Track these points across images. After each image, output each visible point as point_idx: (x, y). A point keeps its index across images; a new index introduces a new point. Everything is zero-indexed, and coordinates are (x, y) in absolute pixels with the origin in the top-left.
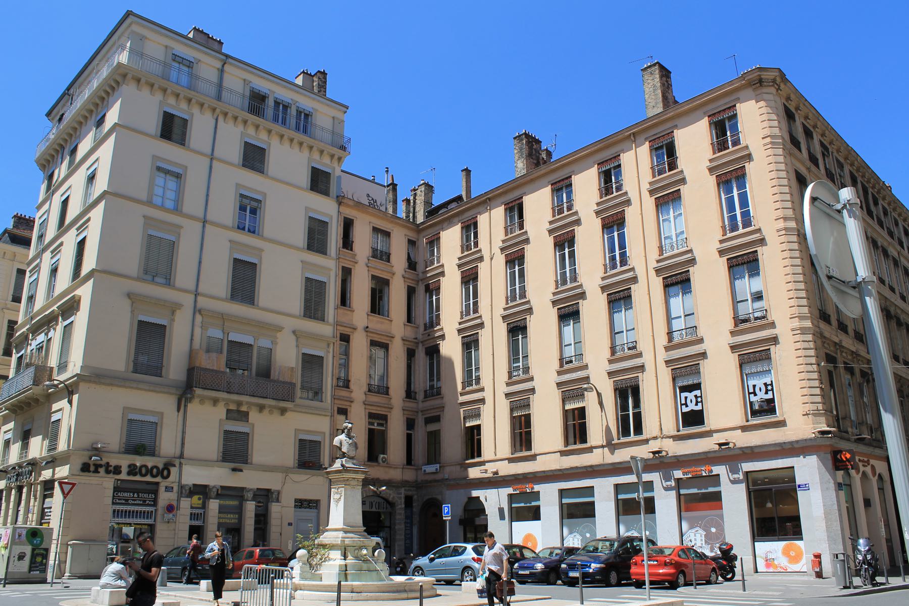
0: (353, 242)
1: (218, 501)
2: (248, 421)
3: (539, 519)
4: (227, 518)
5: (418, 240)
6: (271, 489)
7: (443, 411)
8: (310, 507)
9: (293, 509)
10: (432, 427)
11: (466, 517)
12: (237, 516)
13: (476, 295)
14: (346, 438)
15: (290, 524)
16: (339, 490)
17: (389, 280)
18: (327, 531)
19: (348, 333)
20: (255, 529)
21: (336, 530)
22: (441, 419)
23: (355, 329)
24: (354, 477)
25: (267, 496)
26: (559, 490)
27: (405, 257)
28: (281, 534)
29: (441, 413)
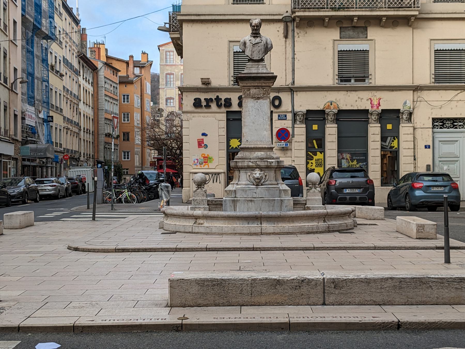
15: (427, 147)
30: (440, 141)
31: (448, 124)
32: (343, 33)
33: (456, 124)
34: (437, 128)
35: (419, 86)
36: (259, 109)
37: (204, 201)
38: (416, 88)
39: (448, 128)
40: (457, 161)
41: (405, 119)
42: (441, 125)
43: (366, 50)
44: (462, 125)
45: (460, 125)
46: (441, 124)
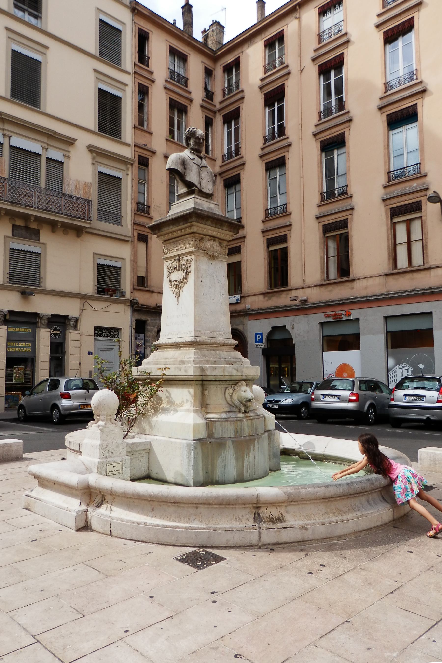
0: (149, 58)
1: (6, 327)
2: (39, 240)
3: (359, 348)
4: (19, 347)
5: (215, 69)
6: (68, 316)
7: (244, 241)
8: (111, 336)
9: (93, 338)
10: (235, 259)
11: (269, 347)
12: (30, 344)
13: (281, 117)
14: (192, 157)
15: (90, 353)
16: (182, 262)
17: (187, 106)
18: (157, 348)
19: (148, 157)
20: (51, 359)
21: (177, 345)
22: (242, 250)
23: (154, 153)
24: (214, 234)
25: (64, 323)
26: (384, 316)
27: (202, 86)
28: (80, 364)
29: (242, 244)
30: (100, 349)
31: (106, 333)
32: (15, 231)
33: (112, 333)
34: (97, 337)
35: (86, 295)
36: (215, 276)
37: (121, 447)
38: (83, 297)
39: (106, 337)
40: (112, 367)
41: (72, 326)
42: (100, 334)
43: (38, 253)
44: (117, 335)
45: (115, 335)
46: (100, 332)
